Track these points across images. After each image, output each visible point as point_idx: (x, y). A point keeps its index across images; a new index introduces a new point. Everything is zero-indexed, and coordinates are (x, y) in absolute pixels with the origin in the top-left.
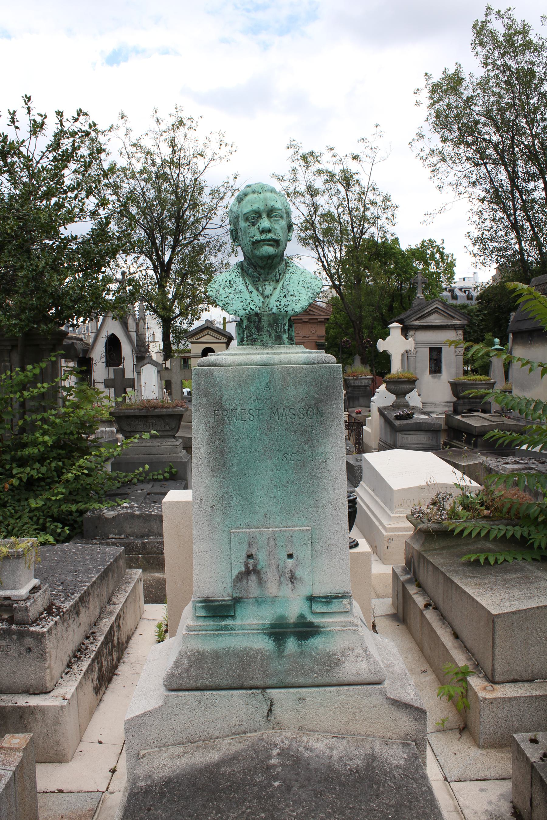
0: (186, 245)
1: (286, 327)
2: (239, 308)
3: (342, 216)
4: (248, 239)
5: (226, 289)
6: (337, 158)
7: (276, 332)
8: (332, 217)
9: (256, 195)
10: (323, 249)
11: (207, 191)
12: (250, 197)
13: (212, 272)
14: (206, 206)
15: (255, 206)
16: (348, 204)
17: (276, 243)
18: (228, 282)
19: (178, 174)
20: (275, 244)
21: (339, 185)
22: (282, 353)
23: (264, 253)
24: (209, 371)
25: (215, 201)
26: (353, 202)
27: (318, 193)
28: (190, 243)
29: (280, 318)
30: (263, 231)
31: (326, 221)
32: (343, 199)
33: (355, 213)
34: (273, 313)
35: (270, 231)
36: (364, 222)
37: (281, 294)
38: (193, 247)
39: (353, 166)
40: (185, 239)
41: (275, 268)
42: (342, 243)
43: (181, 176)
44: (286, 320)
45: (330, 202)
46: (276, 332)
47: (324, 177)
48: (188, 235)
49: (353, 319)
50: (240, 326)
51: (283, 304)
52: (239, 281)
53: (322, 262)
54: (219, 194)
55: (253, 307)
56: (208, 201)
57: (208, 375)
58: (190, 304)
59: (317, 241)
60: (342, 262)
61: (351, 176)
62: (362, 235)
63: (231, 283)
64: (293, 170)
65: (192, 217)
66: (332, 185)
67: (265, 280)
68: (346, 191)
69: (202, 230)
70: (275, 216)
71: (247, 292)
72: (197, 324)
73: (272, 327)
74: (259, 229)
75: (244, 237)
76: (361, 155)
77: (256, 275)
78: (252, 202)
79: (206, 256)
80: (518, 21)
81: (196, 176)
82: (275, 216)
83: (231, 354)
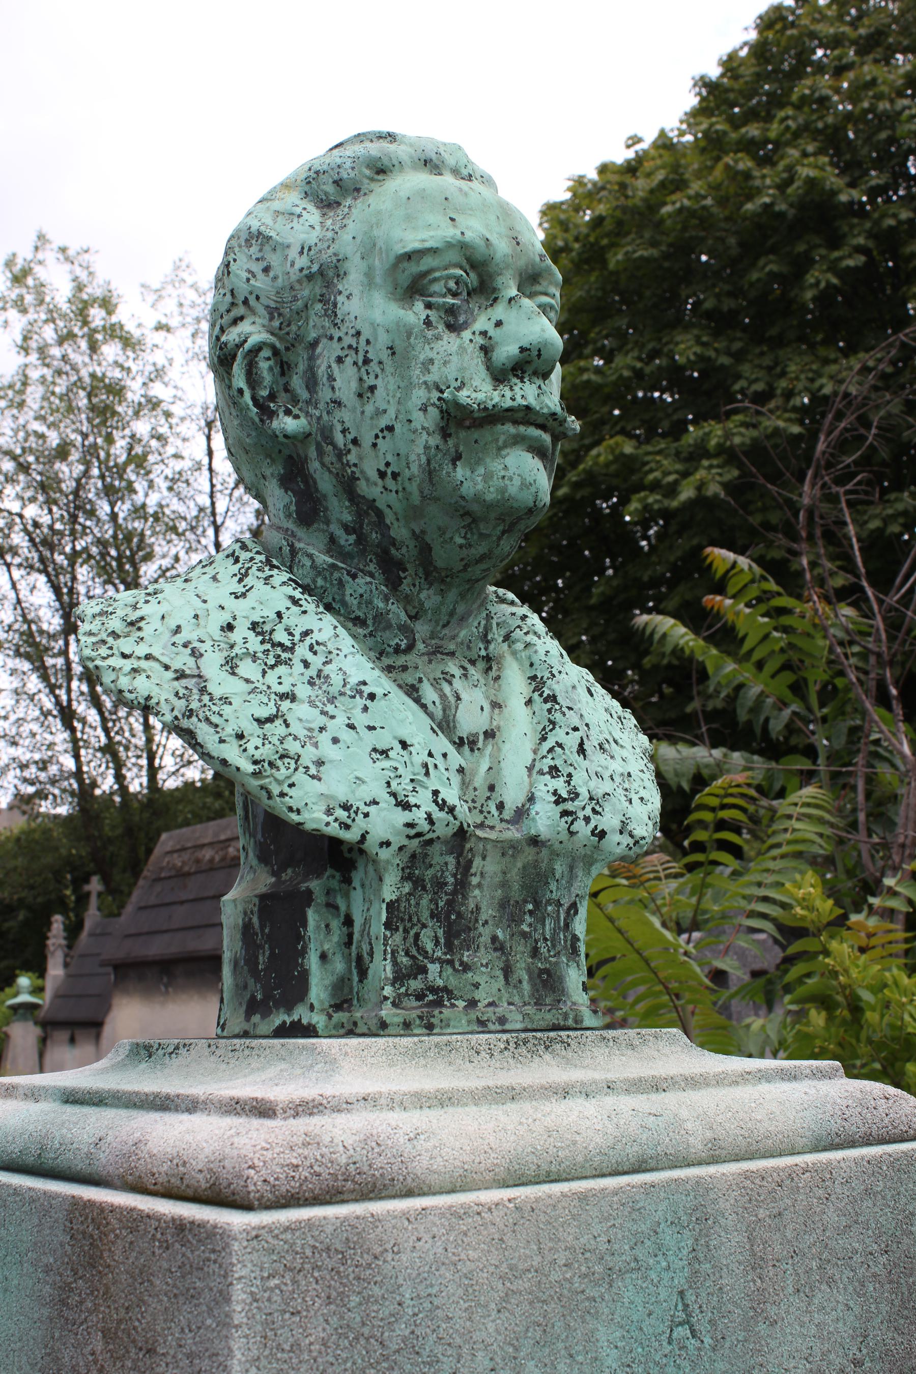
7: (535, 953)
12: (413, 181)
23: (513, 489)
24: (353, 1237)
29: (560, 868)
34: (534, 841)
46: (535, 953)
55: (451, 795)
57: (344, 1266)
73: (515, 920)
74: (486, 350)
77: (397, 612)
80: (100, 279)
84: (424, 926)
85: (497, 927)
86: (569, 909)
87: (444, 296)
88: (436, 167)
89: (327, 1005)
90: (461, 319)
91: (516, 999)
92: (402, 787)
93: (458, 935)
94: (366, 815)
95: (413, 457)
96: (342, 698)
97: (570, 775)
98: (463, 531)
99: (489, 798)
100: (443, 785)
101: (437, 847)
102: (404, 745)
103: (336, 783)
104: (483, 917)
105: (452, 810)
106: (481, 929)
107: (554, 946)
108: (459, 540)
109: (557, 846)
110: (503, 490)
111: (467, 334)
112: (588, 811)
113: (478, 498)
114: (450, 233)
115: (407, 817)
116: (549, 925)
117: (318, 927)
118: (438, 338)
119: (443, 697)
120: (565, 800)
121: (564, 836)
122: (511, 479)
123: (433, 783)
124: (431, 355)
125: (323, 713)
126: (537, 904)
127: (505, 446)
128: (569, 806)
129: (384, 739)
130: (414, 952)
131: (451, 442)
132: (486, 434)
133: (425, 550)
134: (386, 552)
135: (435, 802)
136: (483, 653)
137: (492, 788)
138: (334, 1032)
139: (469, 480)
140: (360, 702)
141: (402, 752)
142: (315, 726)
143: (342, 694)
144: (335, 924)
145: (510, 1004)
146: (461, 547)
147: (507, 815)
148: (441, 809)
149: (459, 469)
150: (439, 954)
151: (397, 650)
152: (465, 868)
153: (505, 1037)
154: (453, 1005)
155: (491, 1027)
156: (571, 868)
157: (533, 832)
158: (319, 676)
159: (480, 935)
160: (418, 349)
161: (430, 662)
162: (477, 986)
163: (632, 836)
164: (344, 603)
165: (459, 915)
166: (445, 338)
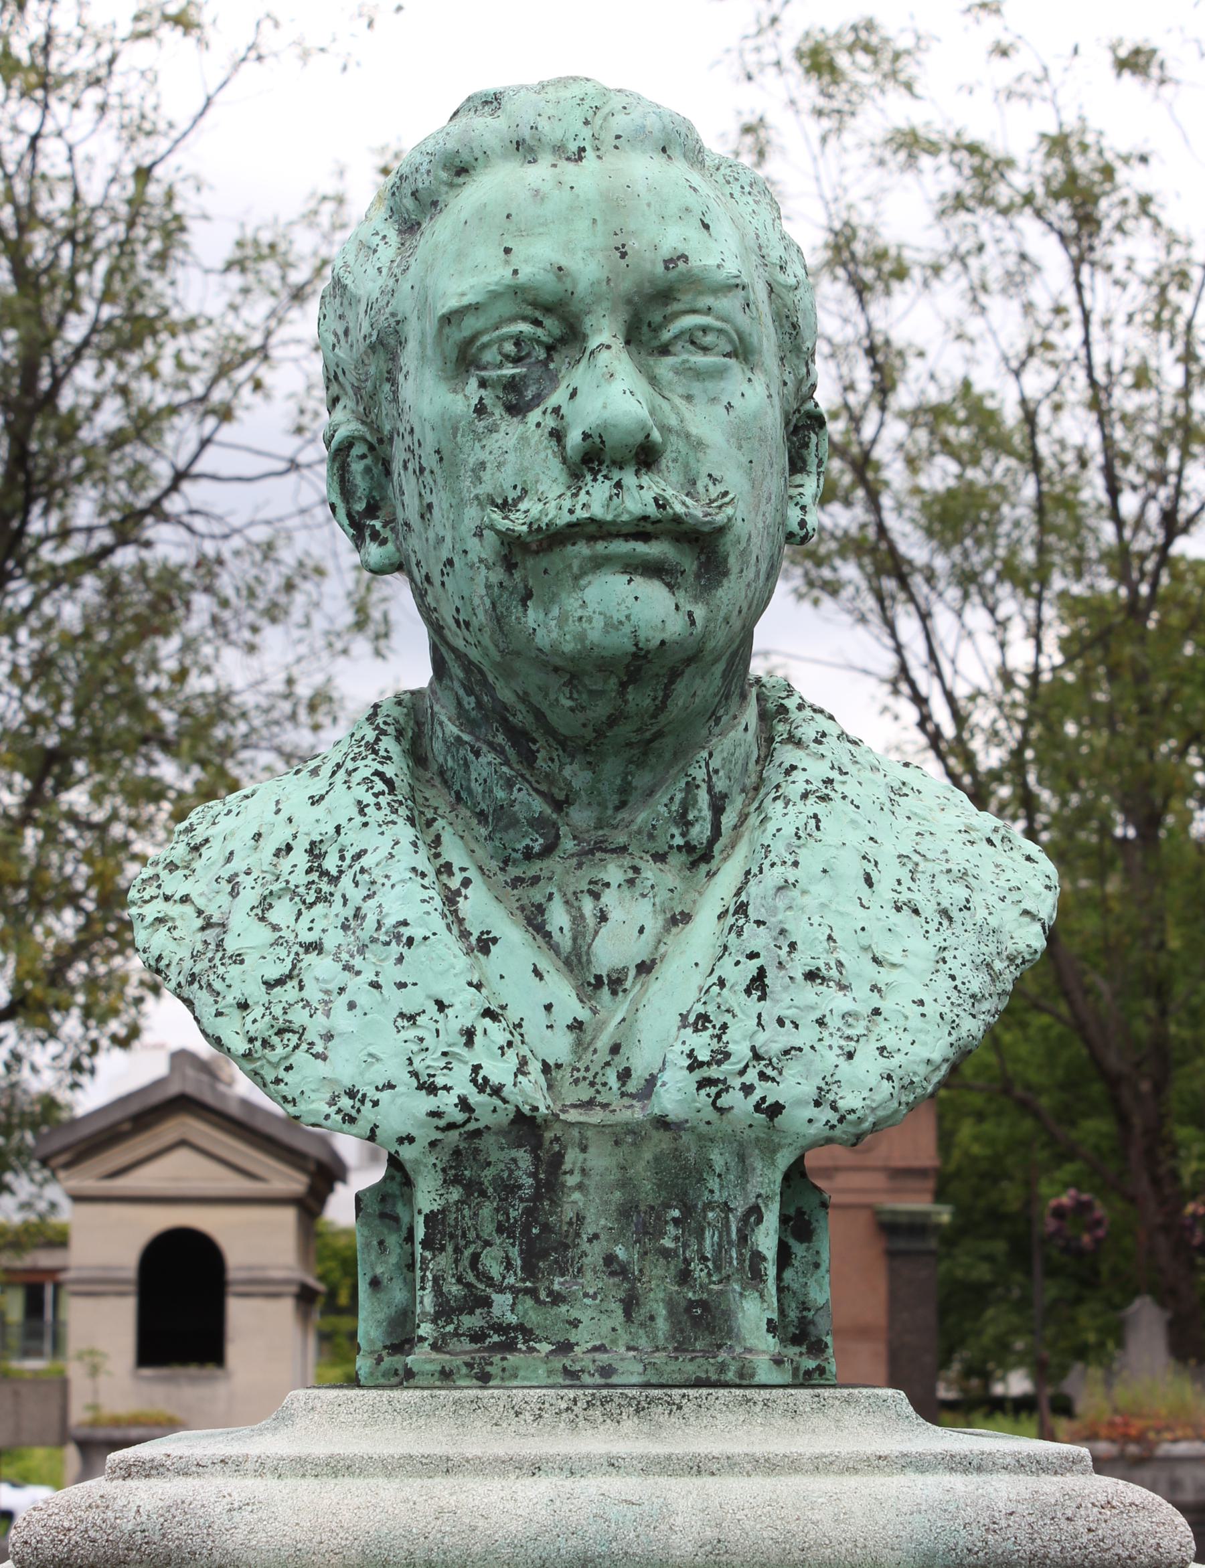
0: (63, 578)
1: (766, 1239)
2: (379, 1074)
3: (1044, 416)
4: (472, 516)
5: (282, 912)
6: (1022, 61)
7: (684, 1277)
8: (982, 416)
9: (540, 173)
10: (925, 617)
11: (209, 243)
13: (226, 749)
14: (201, 339)
15: (535, 260)
16: (1087, 343)
17: (694, 550)
18: (300, 857)
19: (35, 138)
20: (690, 565)
21: (1026, 221)
22: (730, 1465)
23: (595, 634)
25: (257, 310)
26: (1120, 331)
27: (901, 273)
28: (92, 561)
29: (718, 1158)
30: (593, 458)
31: (948, 447)
32: (1059, 310)
33: (1125, 400)
34: (662, 1123)
35: (646, 456)
36: (1186, 455)
37: (726, 969)
38: (113, 588)
39: (1117, 116)
40: (64, 534)
41: (682, 754)
42: (1044, 583)
43: (52, 148)
44: (767, 1179)
45: (975, 326)
46: (684, 1277)
47: (942, 176)
48: (84, 508)
49: (1113, 1061)
50: (389, 1218)
51: (740, 1051)
52: (390, 849)
53: (919, 700)
54: (286, 266)
55: (499, 1071)
56: (214, 306)
58: (79, 949)
59: (887, 564)
60: (1042, 702)
61: (1108, 172)
62: (1169, 541)
63: (323, 869)
64: (748, 130)
65: (113, 404)
66: (986, 224)
67: (596, 849)
68: (1077, 264)
69: (174, 487)
70: (692, 339)
71: (448, 947)
72: (118, 1076)
74: (557, 435)
75: (440, 500)
76: (1169, 49)
78: (509, 224)
79: (189, 646)
81: (145, 151)
82: (692, 339)
83: (303, 1467)
84: (488, 1244)
85: (616, 1242)
86: (745, 1218)
87: (500, 366)
88: (531, 150)
89: (379, 1345)
90: (529, 394)
91: (643, 1342)
92: (430, 1062)
93: (544, 1255)
94: (376, 1104)
95: (477, 601)
96: (372, 946)
97: (724, 1027)
98: (567, 690)
99: (608, 1064)
100: (491, 1056)
102: (441, 1006)
103: (344, 1066)
104: (589, 1229)
105: (497, 1091)
107: (718, 1268)
108: (568, 703)
109: (703, 1128)
110: (581, 637)
111: (534, 416)
112: (751, 1076)
113: (555, 649)
114: (496, 274)
115: (431, 1103)
116: (710, 1240)
117: (367, 1245)
118: (493, 429)
119: (578, 919)
120: (701, 1064)
121: (709, 1114)
122: (590, 620)
123: (473, 1057)
124: (483, 456)
125: (347, 968)
126: (688, 1210)
127: (583, 573)
128: (714, 1072)
129: (412, 1000)
130: (470, 1277)
131: (517, 575)
132: (554, 560)
133: (539, 716)
134: (506, 720)
135: (474, 1081)
136: (679, 841)
137: (615, 1049)
138: (382, 1381)
139: (543, 625)
140: (395, 949)
141: (437, 1016)
142: (333, 987)
143: (374, 940)
144: (393, 1240)
145: (629, 1348)
146: (572, 710)
147: (632, 1086)
148: (481, 1090)
149: (530, 612)
150: (511, 1280)
151: (528, 855)
153: (571, 1393)
154: (532, 1350)
155: (586, 1379)
156: (742, 1158)
157: (657, 1111)
158: (356, 916)
159: (584, 1254)
160: (466, 450)
161: (580, 866)
162: (575, 1323)
163: (834, 1108)
164: (470, 791)
165: (546, 1228)
166: (503, 428)
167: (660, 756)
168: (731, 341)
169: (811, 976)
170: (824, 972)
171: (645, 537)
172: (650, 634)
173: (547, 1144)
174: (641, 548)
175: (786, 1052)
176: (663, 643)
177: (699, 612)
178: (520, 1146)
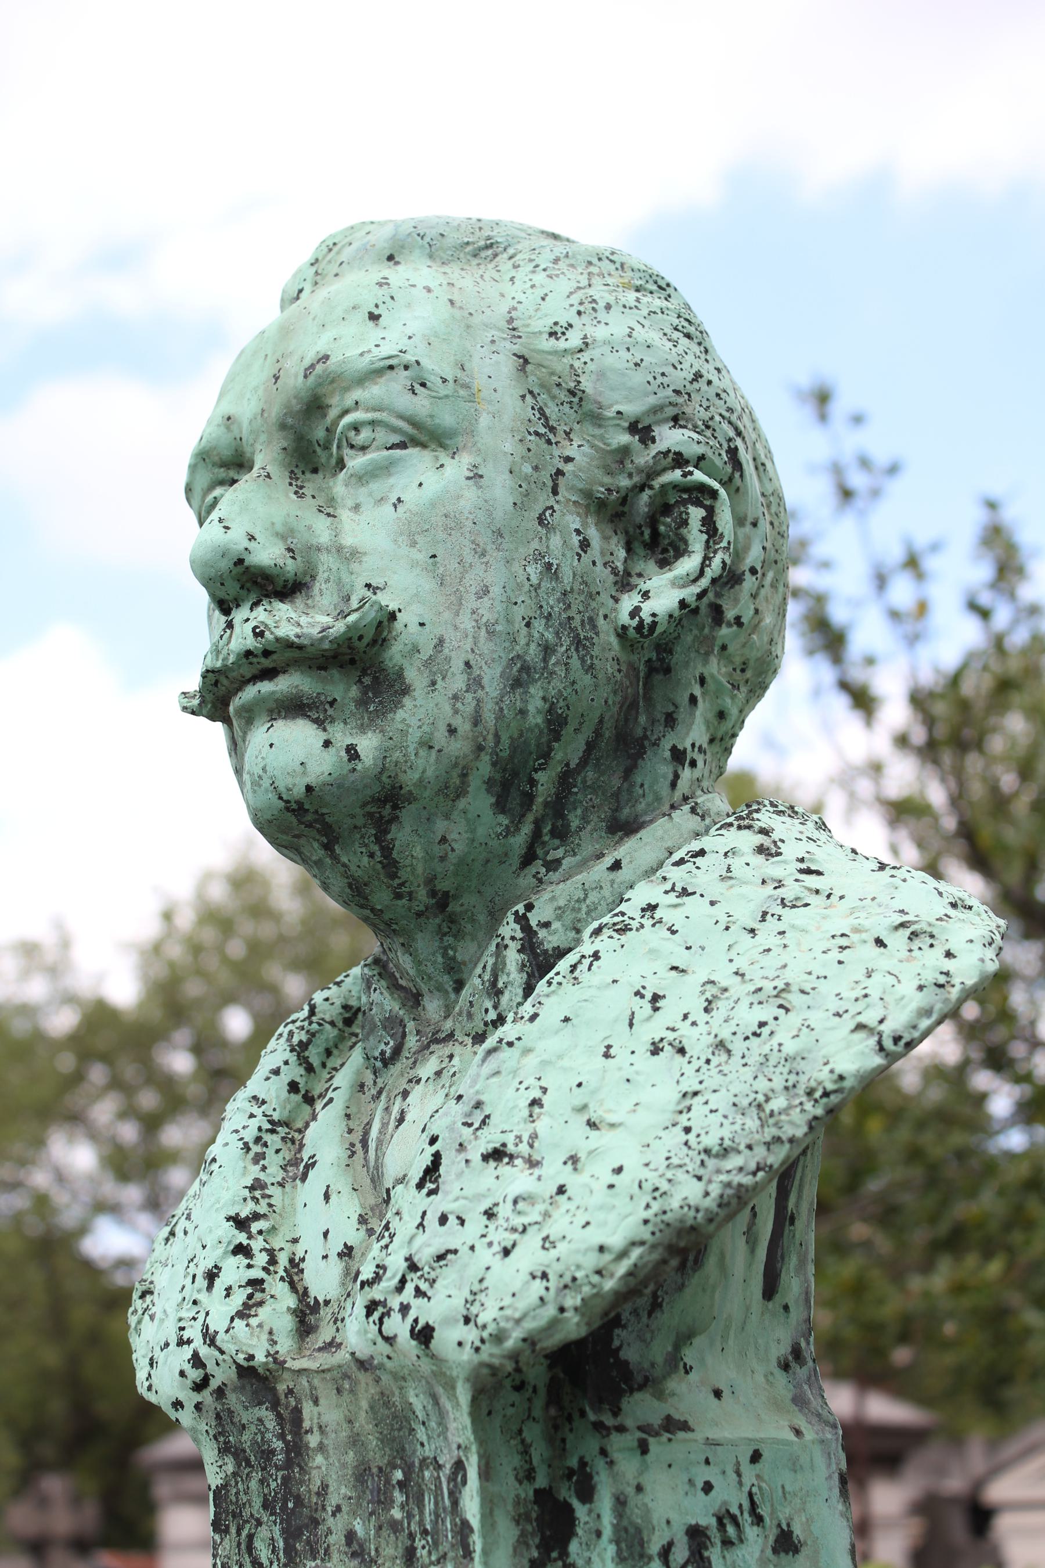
29: (418, 1402)
84: (259, 1523)
86: (452, 1478)
101: (233, 1399)
104: (333, 1500)
106: (330, 1521)
107: (436, 1544)
152: (292, 1423)
159: (330, 1532)
165: (299, 1500)
167: (473, 920)
168: (395, 430)
169: (497, 1155)
170: (511, 1148)
171: (269, 674)
172: (289, 782)
173: (283, 1400)
174: (266, 687)
175: (440, 1257)
176: (309, 789)
177: (368, 744)
178: (260, 1403)
